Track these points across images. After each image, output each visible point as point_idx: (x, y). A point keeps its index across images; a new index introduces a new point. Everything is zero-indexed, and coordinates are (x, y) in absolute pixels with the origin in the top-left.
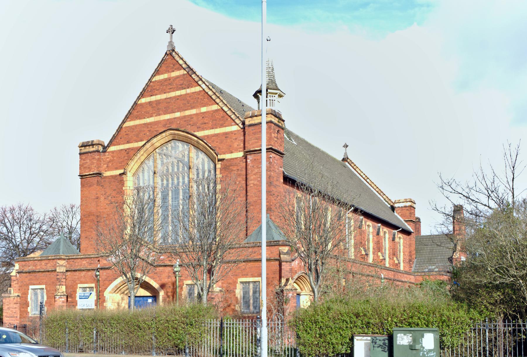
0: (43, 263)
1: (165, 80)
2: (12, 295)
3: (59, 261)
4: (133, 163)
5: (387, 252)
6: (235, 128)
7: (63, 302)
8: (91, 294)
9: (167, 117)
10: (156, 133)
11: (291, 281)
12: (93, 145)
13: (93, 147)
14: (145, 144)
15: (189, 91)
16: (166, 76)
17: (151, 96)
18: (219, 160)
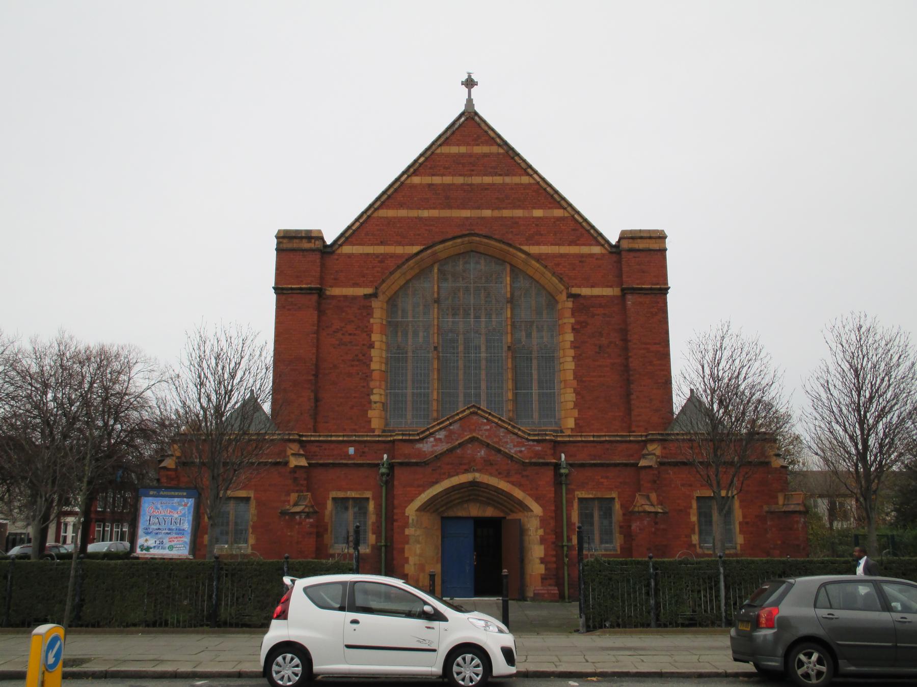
9: (466, 213)
13: (310, 242)
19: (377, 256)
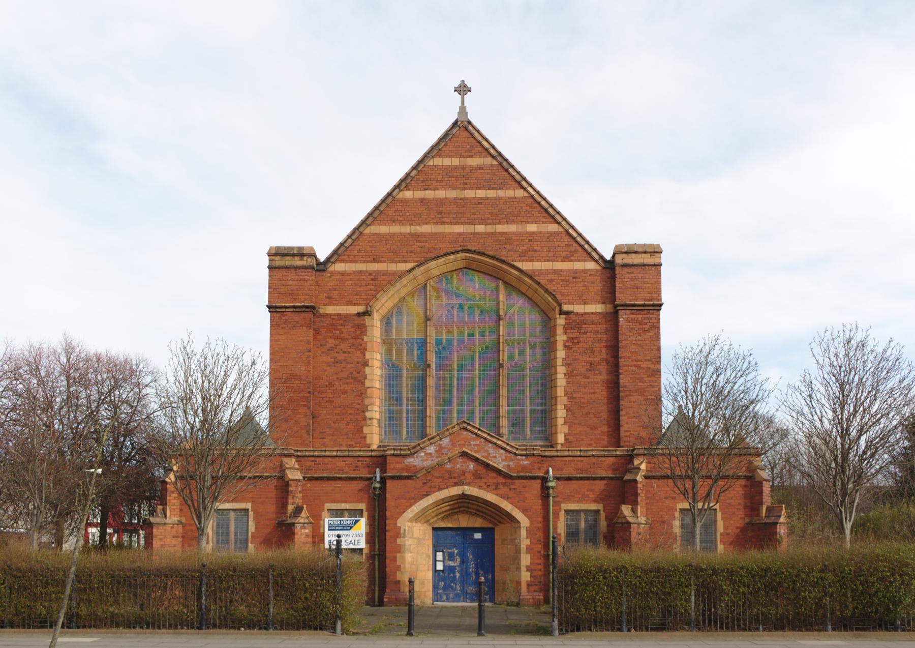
1: (455, 168)
2: (168, 521)
4: (386, 298)
7: (307, 536)
8: (357, 522)
9: (459, 229)
10: (437, 253)
13: (302, 259)
14: (414, 268)
15: (502, 193)
17: (426, 189)
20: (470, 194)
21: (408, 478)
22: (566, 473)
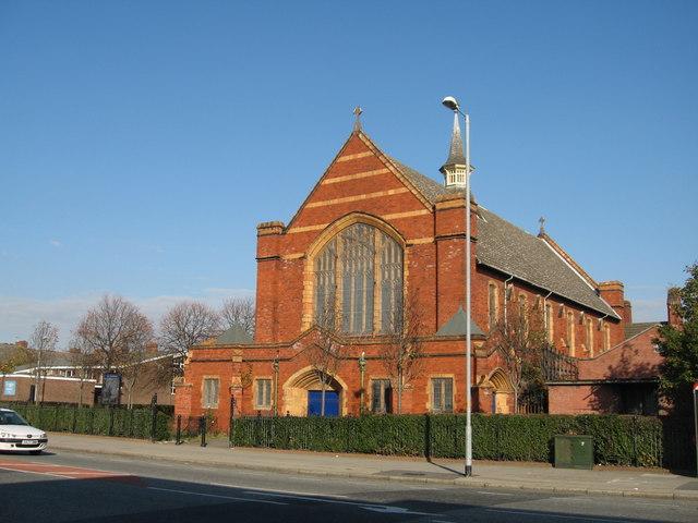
0: (219, 351)
1: (351, 161)
3: (235, 351)
5: (592, 343)
6: (424, 212)
9: (352, 199)
11: (487, 378)
12: (272, 227)
16: (351, 157)
18: (407, 246)
19: (307, 233)
20: (358, 176)
21: (288, 360)
22: (371, 355)
